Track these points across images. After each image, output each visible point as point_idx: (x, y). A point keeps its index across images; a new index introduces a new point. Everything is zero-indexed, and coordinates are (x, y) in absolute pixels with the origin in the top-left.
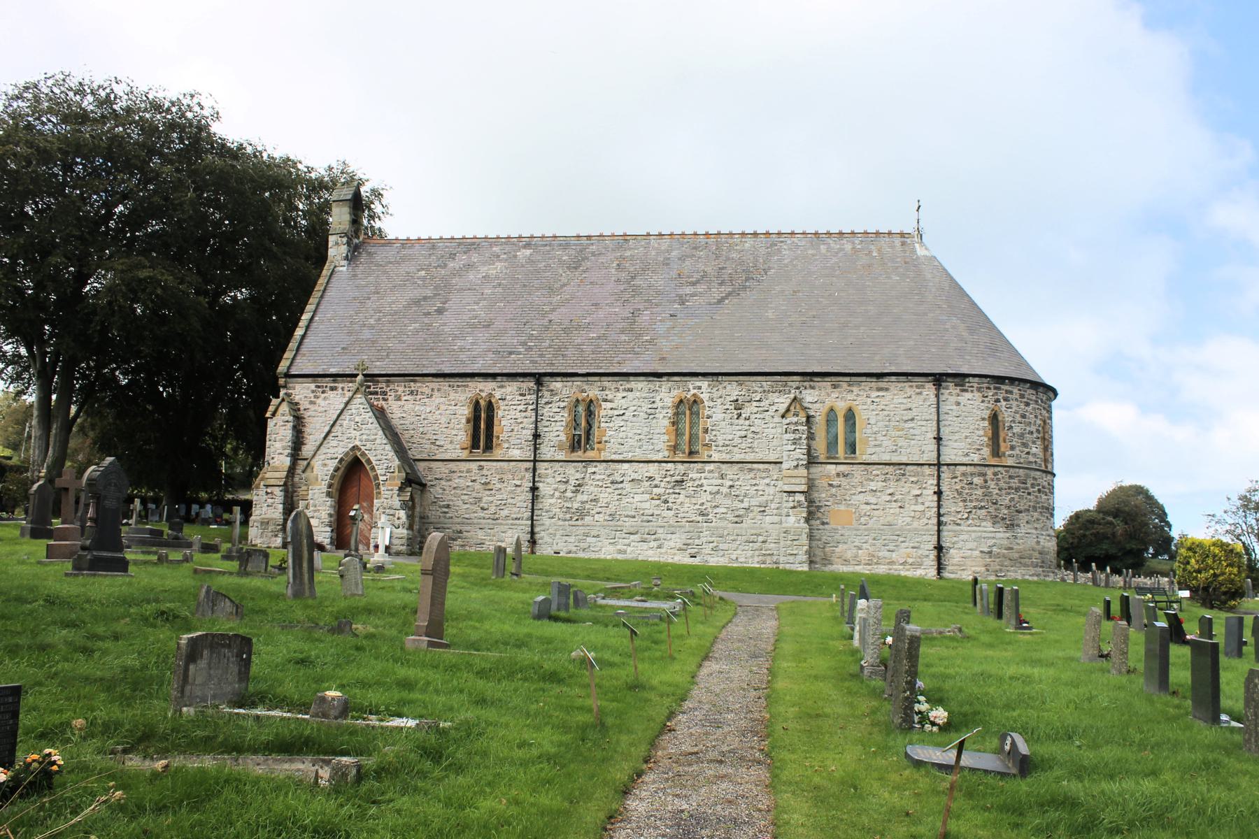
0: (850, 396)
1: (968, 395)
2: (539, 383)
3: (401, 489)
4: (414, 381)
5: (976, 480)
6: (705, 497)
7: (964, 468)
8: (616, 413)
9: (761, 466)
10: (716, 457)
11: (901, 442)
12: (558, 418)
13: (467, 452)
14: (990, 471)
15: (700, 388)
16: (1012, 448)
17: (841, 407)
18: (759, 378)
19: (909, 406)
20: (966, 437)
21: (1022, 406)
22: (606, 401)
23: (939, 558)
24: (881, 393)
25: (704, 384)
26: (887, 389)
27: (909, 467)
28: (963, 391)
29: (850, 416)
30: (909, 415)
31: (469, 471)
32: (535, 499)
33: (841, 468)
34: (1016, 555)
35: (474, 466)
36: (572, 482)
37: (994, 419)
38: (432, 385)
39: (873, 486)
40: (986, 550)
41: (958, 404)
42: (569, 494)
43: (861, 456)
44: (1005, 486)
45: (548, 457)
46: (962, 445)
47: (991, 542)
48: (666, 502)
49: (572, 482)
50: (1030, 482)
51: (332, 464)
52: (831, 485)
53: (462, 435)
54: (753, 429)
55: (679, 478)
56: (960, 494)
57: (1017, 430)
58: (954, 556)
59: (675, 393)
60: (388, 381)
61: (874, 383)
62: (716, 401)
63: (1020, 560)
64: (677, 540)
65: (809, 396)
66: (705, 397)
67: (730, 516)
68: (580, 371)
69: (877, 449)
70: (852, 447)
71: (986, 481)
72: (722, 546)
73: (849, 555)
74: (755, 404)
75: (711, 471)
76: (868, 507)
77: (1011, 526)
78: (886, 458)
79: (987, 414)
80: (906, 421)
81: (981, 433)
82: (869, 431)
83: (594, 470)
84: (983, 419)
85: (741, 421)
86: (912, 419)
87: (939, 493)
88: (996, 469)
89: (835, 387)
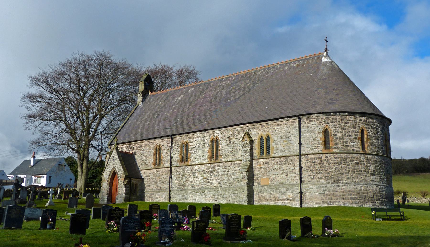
0: (267, 130)
1: (312, 123)
2: (172, 139)
3: (124, 181)
4: (141, 142)
5: (317, 161)
6: (220, 177)
7: (310, 156)
8: (194, 146)
9: (237, 162)
10: (223, 160)
11: (287, 147)
12: (177, 151)
13: (154, 166)
14: (323, 156)
15: (218, 134)
16: (336, 144)
17: (264, 135)
18: (236, 127)
19: (289, 130)
20: (312, 142)
21: (343, 124)
22: (191, 142)
23: (301, 197)
24: (278, 127)
25: (219, 131)
26: (280, 125)
27: (290, 158)
28: (310, 121)
29: (268, 138)
30: (289, 134)
31: (154, 173)
32: (170, 182)
33: (265, 160)
34: (339, 195)
35: (155, 170)
36: (181, 174)
37: (326, 133)
38: (146, 143)
39: (276, 167)
40: (322, 192)
41: (308, 127)
42: (180, 179)
43: (272, 155)
44: (332, 162)
45: (175, 165)
46: (310, 145)
47: (324, 189)
48: (208, 179)
49: (181, 174)
50: (348, 160)
51: (108, 173)
52: (261, 168)
53: (152, 160)
54: (235, 148)
55: (211, 170)
56: (309, 167)
57: (339, 135)
58: (307, 195)
59: (211, 136)
60: (134, 144)
61: (274, 123)
62: (173, 137)
63: (343, 196)
64: (211, 194)
65: (253, 132)
66: (219, 137)
67: (228, 184)
68: (183, 133)
69: (278, 151)
70: (268, 152)
71: (321, 161)
72: (225, 196)
73: (267, 197)
74: (235, 137)
75: (222, 166)
76: (274, 176)
77: (336, 181)
78: (281, 154)
79: (322, 130)
80: (288, 137)
81: (319, 139)
82: (274, 143)
83: (187, 169)
84: (320, 133)
85: (231, 145)
86: (290, 136)
87: (301, 168)
88: (327, 155)
89: (262, 127)
